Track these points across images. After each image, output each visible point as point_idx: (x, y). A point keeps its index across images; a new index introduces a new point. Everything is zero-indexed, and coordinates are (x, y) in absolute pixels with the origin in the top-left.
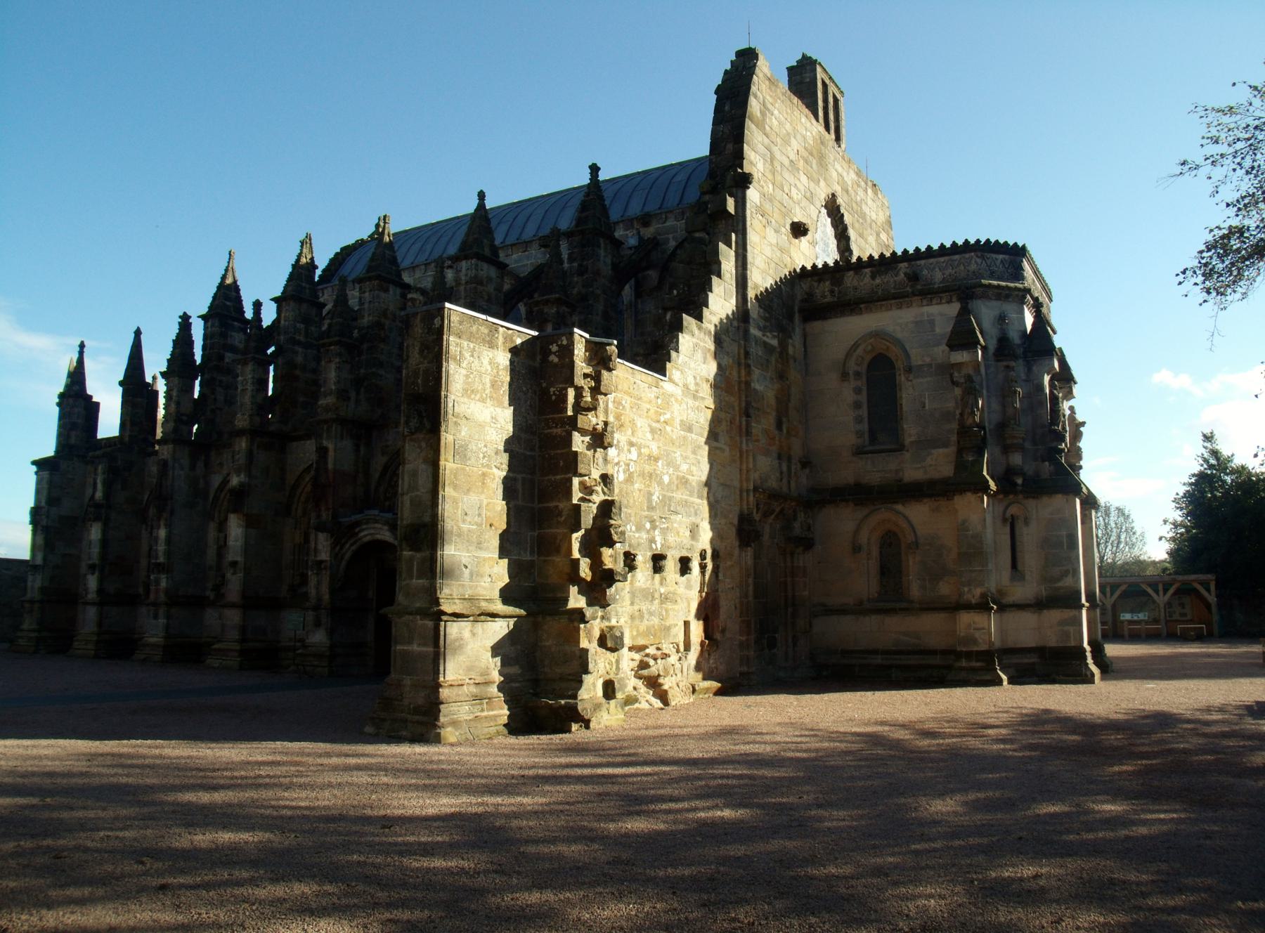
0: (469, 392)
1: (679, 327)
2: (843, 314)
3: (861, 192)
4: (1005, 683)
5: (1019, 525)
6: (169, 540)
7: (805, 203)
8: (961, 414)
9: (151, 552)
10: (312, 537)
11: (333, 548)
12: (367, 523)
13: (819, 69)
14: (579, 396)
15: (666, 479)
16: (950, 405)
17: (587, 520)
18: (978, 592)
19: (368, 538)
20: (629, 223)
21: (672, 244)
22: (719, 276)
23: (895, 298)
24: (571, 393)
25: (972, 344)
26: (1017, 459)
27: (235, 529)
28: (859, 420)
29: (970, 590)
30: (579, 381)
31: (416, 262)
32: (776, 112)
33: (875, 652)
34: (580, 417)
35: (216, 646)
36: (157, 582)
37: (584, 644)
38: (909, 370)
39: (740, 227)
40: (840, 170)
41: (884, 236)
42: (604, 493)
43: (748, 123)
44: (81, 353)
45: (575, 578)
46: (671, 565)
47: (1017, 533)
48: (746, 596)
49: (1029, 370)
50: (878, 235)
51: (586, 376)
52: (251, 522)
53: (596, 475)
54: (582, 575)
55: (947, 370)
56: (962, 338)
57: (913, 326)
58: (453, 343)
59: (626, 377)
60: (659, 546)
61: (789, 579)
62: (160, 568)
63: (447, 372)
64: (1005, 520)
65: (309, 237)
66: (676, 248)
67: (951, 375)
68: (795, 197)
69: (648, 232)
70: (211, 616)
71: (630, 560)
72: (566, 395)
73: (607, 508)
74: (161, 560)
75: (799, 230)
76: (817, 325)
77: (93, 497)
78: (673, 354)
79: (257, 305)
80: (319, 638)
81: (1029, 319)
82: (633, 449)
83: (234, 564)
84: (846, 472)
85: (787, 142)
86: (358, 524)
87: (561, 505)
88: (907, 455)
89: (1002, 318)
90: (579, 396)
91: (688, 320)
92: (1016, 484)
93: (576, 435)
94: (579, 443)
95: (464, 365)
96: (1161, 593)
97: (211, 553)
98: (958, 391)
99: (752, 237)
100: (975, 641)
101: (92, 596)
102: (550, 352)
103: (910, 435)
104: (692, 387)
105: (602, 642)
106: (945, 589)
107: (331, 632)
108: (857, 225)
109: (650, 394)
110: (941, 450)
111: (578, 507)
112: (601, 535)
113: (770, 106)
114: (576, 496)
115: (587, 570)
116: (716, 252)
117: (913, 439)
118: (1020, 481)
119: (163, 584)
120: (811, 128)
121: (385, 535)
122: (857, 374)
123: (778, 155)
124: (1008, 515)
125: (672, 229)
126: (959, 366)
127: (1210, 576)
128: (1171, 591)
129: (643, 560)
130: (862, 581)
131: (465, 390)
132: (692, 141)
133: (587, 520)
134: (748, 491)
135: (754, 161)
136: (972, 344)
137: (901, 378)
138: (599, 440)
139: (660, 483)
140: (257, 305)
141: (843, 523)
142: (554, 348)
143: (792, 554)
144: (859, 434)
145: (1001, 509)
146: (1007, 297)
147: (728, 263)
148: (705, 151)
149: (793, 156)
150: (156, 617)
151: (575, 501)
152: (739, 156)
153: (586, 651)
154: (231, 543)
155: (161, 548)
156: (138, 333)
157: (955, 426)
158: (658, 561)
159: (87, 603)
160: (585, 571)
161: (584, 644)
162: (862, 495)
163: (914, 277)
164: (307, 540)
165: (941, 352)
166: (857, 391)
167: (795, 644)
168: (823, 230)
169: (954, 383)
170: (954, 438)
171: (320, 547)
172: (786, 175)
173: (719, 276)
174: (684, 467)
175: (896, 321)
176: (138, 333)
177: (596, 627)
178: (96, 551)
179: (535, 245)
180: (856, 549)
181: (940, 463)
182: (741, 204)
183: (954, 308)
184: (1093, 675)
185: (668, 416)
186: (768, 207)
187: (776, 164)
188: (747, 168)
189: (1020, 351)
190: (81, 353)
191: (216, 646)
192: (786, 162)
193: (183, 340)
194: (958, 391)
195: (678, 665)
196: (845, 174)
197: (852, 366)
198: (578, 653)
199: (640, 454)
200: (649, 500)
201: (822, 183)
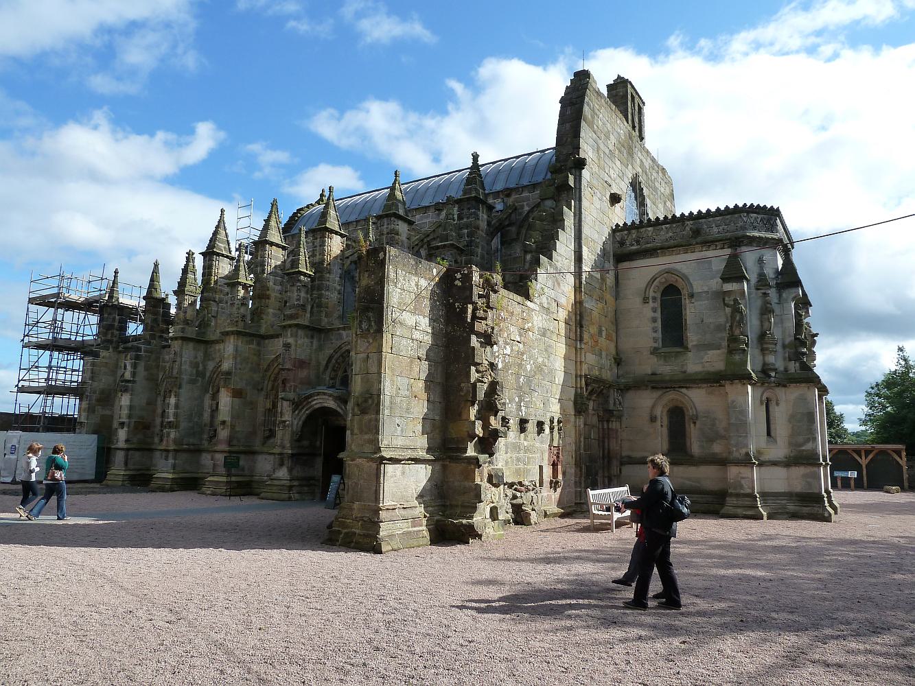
1: (537, 263)
3: (655, 174)
4: (765, 518)
6: (177, 406)
7: (618, 180)
8: (731, 327)
10: (279, 404)
13: (629, 86)
16: (722, 320)
17: (481, 395)
20: (496, 194)
21: (527, 208)
22: (563, 230)
24: (470, 308)
25: (741, 278)
26: (771, 359)
27: (225, 400)
29: (737, 450)
30: (475, 298)
31: (349, 220)
32: (601, 116)
34: (476, 323)
35: (209, 479)
36: (168, 434)
38: (692, 296)
40: (642, 157)
41: (668, 204)
43: (583, 123)
44: (116, 277)
45: (472, 436)
46: (531, 427)
49: (780, 296)
50: (665, 203)
51: (480, 296)
52: (237, 394)
55: (722, 295)
56: (733, 273)
58: (390, 271)
59: (505, 299)
64: (762, 403)
65: (275, 201)
66: (529, 212)
67: (724, 300)
68: (612, 176)
69: (510, 201)
71: (505, 421)
72: (467, 308)
73: (494, 387)
74: (171, 419)
75: (615, 199)
76: (626, 265)
77: (123, 375)
80: (283, 473)
81: (780, 262)
82: (507, 347)
83: (224, 423)
84: (647, 365)
85: (608, 137)
86: (311, 396)
88: (690, 354)
89: (760, 261)
90: (475, 309)
91: (543, 259)
92: (770, 376)
93: (474, 338)
94: (474, 342)
96: (863, 457)
97: (206, 416)
98: (728, 310)
99: (585, 203)
100: (741, 487)
102: (456, 279)
103: (692, 341)
105: (490, 480)
106: (717, 448)
107: (290, 470)
109: (518, 309)
110: (715, 352)
111: (474, 385)
112: (490, 407)
113: (596, 111)
114: (474, 376)
115: (480, 429)
117: (695, 343)
118: (773, 374)
119: (172, 436)
120: (621, 127)
122: (654, 299)
123: (602, 146)
125: (527, 200)
126: (729, 293)
127: (900, 446)
128: (870, 457)
129: (513, 423)
132: (537, 133)
133: (481, 395)
134: (581, 376)
135: (587, 150)
136: (741, 278)
138: (488, 340)
139: (525, 370)
141: (645, 401)
142: (458, 276)
144: (655, 340)
145: (760, 395)
146: (765, 244)
147: (569, 220)
148: (552, 143)
149: (611, 148)
150: (166, 459)
152: (577, 148)
153: (479, 486)
154: (221, 407)
155: (171, 411)
156: (156, 265)
157: (726, 335)
158: (523, 423)
160: (479, 431)
161: (478, 481)
162: (655, 383)
163: (697, 232)
165: (715, 283)
166: (654, 310)
168: (628, 201)
169: (726, 305)
170: (725, 343)
171: (284, 411)
172: (607, 160)
173: (563, 230)
174: (540, 360)
175: (684, 263)
176: (156, 265)
177: (486, 469)
178: (125, 412)
179: (432, 210)
180: (653, 419)
181: (714, 360)
182: (578, 179)
184: (830, 515)
188: (582, 155)
190: (116, 277)
191: (209, 479)
192: (607, 151)
194: (728, 310)
196: (644, 160)
199: (512, 350)
201: (630, 167)
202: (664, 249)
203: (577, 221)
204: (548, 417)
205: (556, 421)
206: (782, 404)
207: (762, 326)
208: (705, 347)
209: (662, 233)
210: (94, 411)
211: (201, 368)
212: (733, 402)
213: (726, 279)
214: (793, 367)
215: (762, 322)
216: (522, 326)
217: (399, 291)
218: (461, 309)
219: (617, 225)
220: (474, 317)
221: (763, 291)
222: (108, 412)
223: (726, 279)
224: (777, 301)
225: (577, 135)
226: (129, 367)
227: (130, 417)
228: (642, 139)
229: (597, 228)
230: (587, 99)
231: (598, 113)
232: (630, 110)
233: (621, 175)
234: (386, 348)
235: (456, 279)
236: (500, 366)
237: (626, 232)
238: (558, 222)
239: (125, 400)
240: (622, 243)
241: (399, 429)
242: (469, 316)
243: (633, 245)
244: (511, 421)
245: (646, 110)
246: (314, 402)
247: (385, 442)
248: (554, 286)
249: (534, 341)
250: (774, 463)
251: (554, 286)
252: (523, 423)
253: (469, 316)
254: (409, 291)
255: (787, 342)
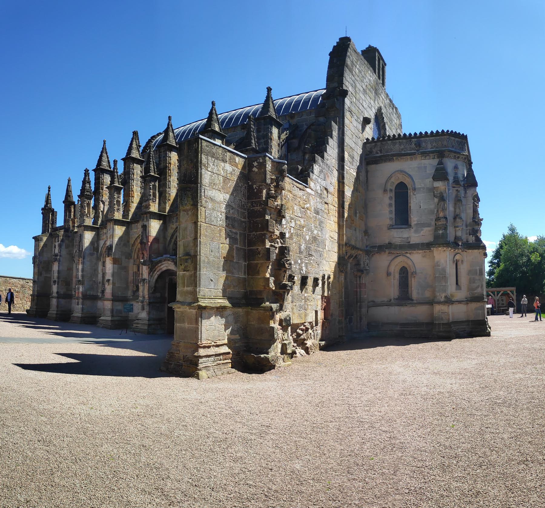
0: (212, 184)
1: (314, 161)
2: (385, 161)
5: (459, 263)
7: (368, 109)
9: (77, 276)
10: (141, 267)
11: (149, 274)
12: (165, 261)
14: (269, 190)
15: (307, 238)
16: (432, 207)
17: (273, 257)
18: (443, 295)
19: (165, 269)
21: (305, 127)
22: (332, 137)
23: (410, 155)
28: (391, 212)
32: (358, 66)
33: (396, 324)
34: (269, 201)
36: (78, 289)
37: (272, 324)
38: (415, 189)
39: (341, 115)
42: (281, 243)
43: (346, 68)
44: (49, 191)
47: (458, 267)
48: (342, 298)
49: (466, 193)
52: (115, 261)
53: (277, 233)
54: (271, 286)
55: (432, 190)
57: (417, 170)
60: (304, 272)
61: (358, 289)
62: (79, 282)
63: (201, 173)
64: (454, 262)
68: (365, 106)
70: (100, 304)
73: (284, 251)
76: (372, 167)
78: (311, 174)
79: (115, 162)
83: (108, 280)
86: (160, 261)
87: (260, 248)
88: (412, 230)
95: (209, 169)
100: (442, 319)
101: (55, 295)
102: (253, 166)
104: (319, 192)
107: (149, 313)
108: (389, 123)
112: (281, 264)
116: (330, 127)
117: (415, 223)
118: (460, 244)
119: (81, 290)
120: (370, 77)
121: (172, 267)
123: (358, 85)
124: (455, 259)
128: (500, 294)
130: (392, 290)
131: (210, 183)
132: (313, 83)
133: (273, 257)
134: (343, 245)
135: (348, 85)
137: (410, 193)
138: (280, 214)
139: (305, 239)
140: (115, 162)
142: (255, 164)
143: (360, 277)
144: (391, 219)
151: (268, 246)
152: (341, 83)
155: (80, 273)
157: (434, 217)
158: (304, 280)
159: (53, 298)
164: (139, 270)
165: (429, 181)
166: (391, 198)
167: (360, 322)
170: (433, 223)
171: (143, 273)
172: (361, 95)
173: (332, 137)
174: (315, 232)
178: (56, 275)
180: (388, 274)
183: (435, 162)
185: (308, 205)
186: (353, 109)
187: (357, 89)
188: (345, 88)
189: (462, 183)
190: (49, 191)
192: (362, 89)
193: (85, 182)
194: (436, 200)
195: (312, 334)
197: (389, 187)
198: (269, 329)
199: (296, 224)
200: (300, 248)
202: (400, 155)
203: (341, 133)
204: (321, 275)
205: (326, 277)
206: (465, 264)
207: (455, 211)
208: (421, 225)
209: (397, 146)
210: (41, 274)
211: (96, 245)
212: (438, 262)
213: (435, 178)
214: (472, 239)
215: (455, 209)
216: (303, 206)
217: (210, 173)
218: (258, 190)
219: (367, 139)
220: (269, 196)
221: (456, 189)
222: (48, 275)
223: (435, 178)
224: (463, 196)
225: (341, 75)
226: (57, 247)
227: (58, 278)
228: (383, 84)
229: (354, 140)
230: (348, 54)
231: (356, 64)
232: (377, 66)
233: (370, 106)
234: (201, 218)
235: (253, 166)
236: (287, 235)
237: (373, 144)
238: (327, 133)
239: (55, 267)
240: (371, 152)
241: (212, 283)
242: (264, 196)
243: (377, 153)
244: (296, 278)
245: (387, 68)
246: (162, 266)
247: (201, 293)
248: (325, 177)
249: (312, 219)
250: (460, 302)
251: (325, 177)
252: (304, 280)
253: (264, 196)
254: (220, 175)
255: (468, 223)
